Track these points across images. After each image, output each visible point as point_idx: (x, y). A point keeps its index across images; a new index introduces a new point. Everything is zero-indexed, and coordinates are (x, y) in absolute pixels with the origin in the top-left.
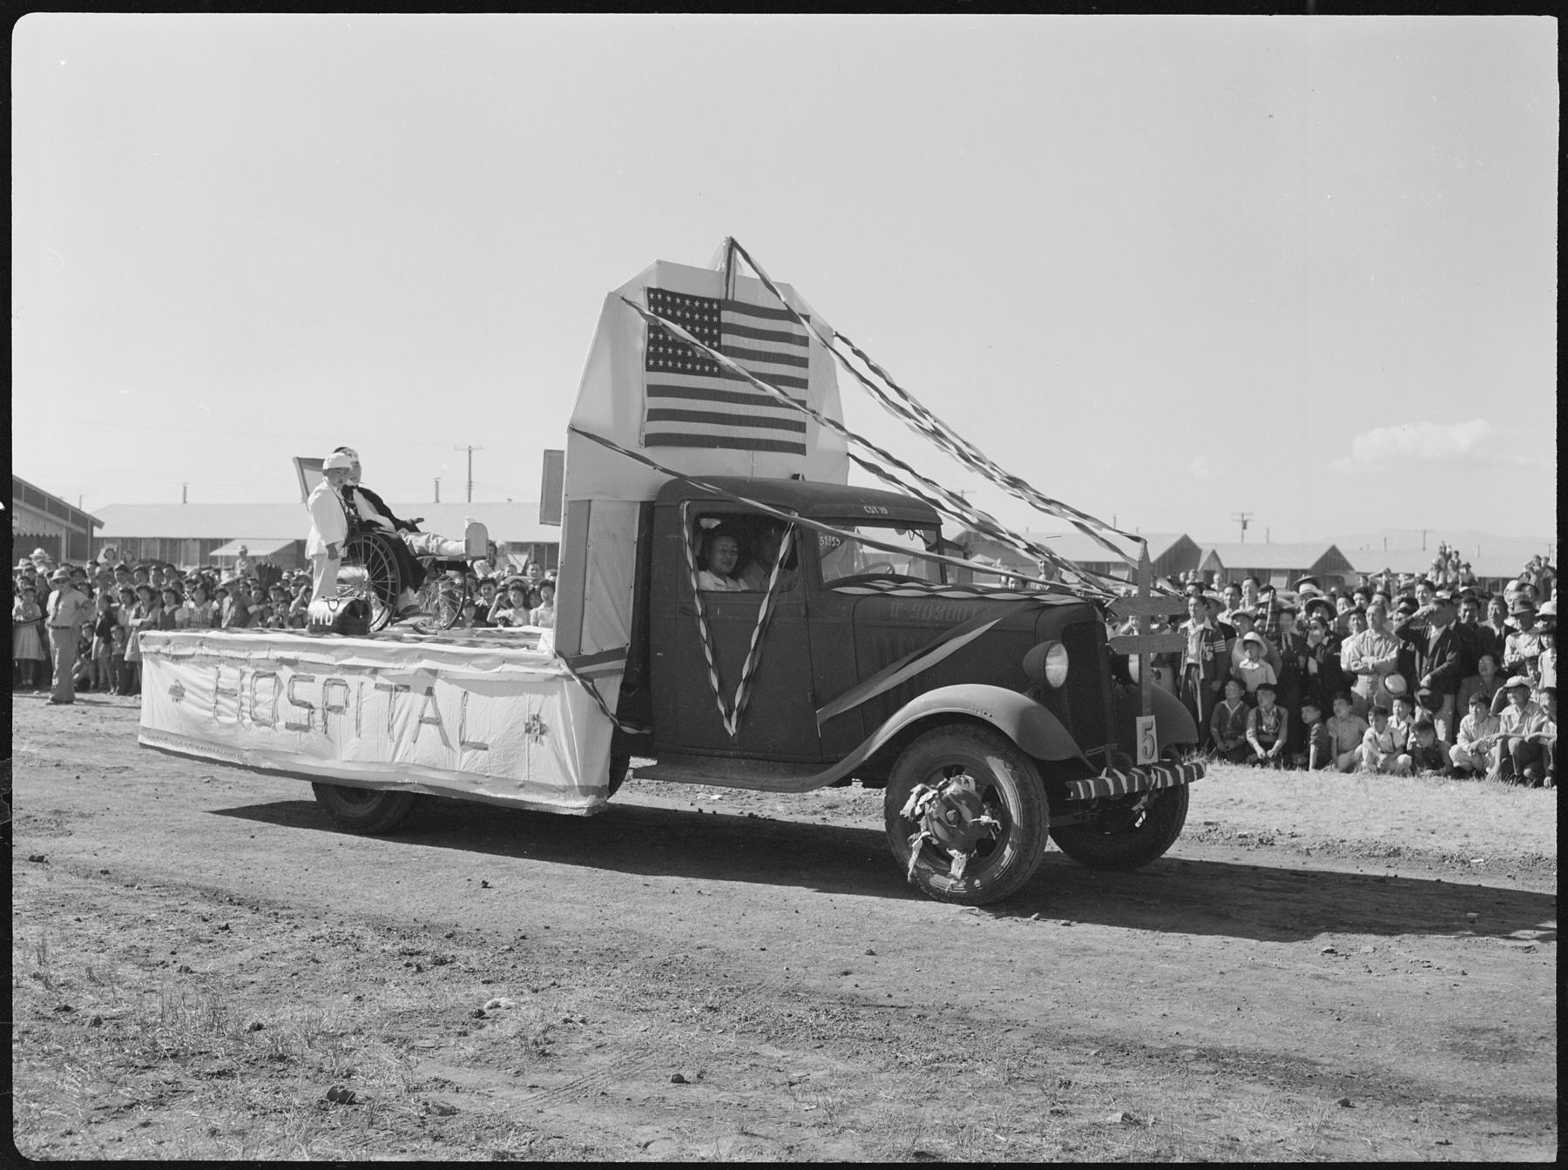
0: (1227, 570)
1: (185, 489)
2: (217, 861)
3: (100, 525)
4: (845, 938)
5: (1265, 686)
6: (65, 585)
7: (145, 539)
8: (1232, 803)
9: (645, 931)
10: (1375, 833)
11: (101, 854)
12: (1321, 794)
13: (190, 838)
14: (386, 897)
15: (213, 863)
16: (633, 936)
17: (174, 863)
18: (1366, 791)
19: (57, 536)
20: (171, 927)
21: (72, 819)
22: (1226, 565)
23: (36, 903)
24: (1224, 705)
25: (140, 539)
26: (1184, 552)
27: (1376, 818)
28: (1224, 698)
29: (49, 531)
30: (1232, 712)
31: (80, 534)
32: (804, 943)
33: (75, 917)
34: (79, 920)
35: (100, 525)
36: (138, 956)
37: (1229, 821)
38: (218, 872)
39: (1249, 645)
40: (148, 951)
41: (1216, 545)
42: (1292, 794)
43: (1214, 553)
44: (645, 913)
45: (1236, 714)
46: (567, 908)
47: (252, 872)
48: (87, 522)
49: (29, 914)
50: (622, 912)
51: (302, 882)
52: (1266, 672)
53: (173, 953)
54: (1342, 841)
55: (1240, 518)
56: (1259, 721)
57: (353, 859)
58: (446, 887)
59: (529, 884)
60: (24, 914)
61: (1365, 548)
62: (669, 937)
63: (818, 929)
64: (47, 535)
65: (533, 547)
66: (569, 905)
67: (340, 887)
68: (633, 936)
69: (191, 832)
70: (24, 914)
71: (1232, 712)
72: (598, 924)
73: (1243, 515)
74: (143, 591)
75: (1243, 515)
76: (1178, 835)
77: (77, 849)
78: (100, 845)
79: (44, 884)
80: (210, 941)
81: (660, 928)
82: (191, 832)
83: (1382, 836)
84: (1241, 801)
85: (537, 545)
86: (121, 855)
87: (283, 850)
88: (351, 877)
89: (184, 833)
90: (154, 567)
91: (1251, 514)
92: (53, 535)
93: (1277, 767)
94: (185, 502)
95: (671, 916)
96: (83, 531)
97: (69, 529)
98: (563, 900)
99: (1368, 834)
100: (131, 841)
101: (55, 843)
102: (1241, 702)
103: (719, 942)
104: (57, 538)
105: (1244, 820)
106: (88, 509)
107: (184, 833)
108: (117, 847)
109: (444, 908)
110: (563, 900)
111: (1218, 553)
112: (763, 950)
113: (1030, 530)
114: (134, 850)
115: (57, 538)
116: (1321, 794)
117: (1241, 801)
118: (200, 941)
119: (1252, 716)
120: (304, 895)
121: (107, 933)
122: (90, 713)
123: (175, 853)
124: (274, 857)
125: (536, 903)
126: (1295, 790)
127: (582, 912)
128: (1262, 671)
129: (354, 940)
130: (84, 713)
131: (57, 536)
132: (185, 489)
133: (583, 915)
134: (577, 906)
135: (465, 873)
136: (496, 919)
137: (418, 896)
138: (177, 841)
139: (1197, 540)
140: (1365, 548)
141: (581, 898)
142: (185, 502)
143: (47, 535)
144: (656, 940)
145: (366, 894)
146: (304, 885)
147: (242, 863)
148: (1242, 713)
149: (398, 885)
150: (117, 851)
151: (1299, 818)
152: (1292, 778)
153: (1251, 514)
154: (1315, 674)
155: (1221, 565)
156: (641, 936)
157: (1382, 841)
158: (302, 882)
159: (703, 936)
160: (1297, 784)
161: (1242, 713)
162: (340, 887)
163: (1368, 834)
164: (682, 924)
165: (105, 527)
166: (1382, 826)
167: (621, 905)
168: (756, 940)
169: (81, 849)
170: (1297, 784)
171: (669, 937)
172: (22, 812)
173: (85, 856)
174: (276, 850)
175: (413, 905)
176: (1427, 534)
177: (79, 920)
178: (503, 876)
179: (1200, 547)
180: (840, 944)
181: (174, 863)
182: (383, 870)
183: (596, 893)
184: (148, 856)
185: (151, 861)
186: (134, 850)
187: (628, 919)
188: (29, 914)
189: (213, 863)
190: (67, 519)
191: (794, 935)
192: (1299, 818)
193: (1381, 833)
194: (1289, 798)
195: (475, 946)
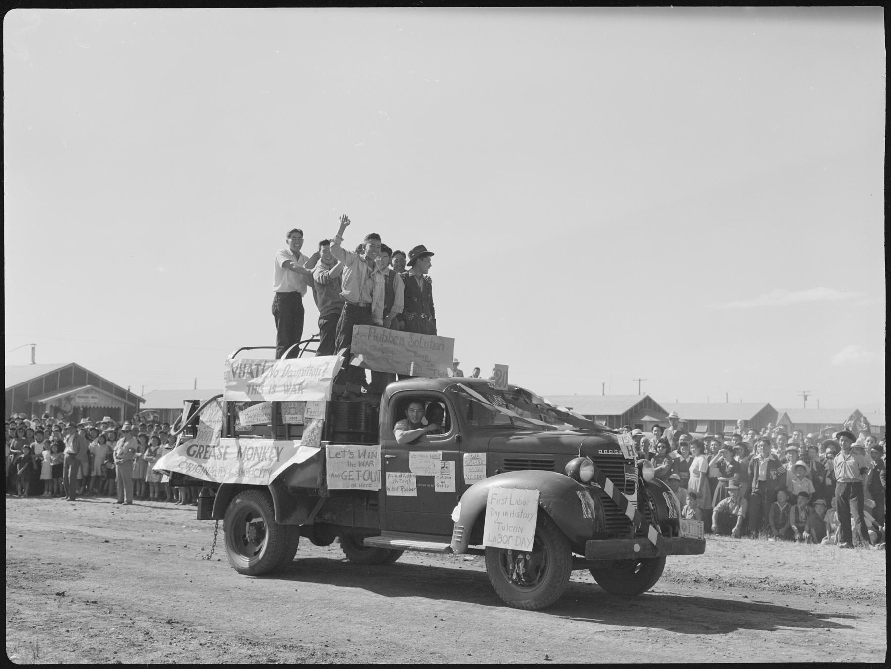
0: (794, 424)
1: (196, 381)
2: (161, 596)
3: (144, 401)
4: (521, 649)
5: (803, 494)
6: (128, 434)
7: (173, 409)
8: (779, 564)
9: (401, 642)
10: (863, 584)
11: (97, 591)
12: (834, 559)
13: (151, 582)
14: (253, 619)
15: (159, 597)
16: (393, 646)
17: (136, 597)
18: (861, 557)
19: (119, 408)
20: (121, 637)
21: (88, 570)
22: (793, 421)
23: (46, 621)
24: (777, 505)
25: (170, 410)
26: (767, 414)
27: (865, 574)
28: (776, 500)
29: (114, 405)
30: (781, 509)
31: (131, 406)
32: (495, 651)
33: (66, 629)
34: (68, 631)
35: (144, 401)
36: (94, 654)
37: (774, 576)
38: (160, 603)
39: (799, 468)
40: (101, 651)
41: (786, 409)
42: (816, 559)
43: (786, 414)
44: (404, 631)
45: (784, 509)
46: (358, 628)
47: (179, 603)
48: (136, 400)
49: (40, 627)
50: (390, 631)
51: (207, 609)
52: (809, 485)
53: (115, 653)
54: (842, 589)
55: (803, 394)
56: (797, 512)
57: (240, 596)
58: (289, 614)
59: (339, 613)
60: (37, 627)
61: (877, 411)
62: (414, 646)
63: (506, 642)
64: (114, 407)
65: (608, 417)
66: (360, 626)
67: (228, 613)
68: (393, 646)
69: (152, 578)
70: (37, 627)
71: (781, 509)
72: (374, 638)
73: (804, 392)
74: (142, 438)
75: (804, 392)
76: (660, 575)
77: (84, 588)
78: (98, 586)
79: (55, 610)
80: (140, 645)
81: (411, 640)
82: (152, 578)
83: (867, 586)
84: (784, 563)
85: (711, 421)
86: (108, 592)
87: (201, 590)
88: (235, 607)
89: (146, 579)
90: (156, 424)
91: (809, 392)
92: (117, 407)
93: (808, 542)
94: (195, 389)
95: (419, 633)
96: (133, 405)
97: (125, 403)
98: (358, 623)
99: (859, 584)
100: (116, 584)
101: (73, 584)
102: (787, 503)
103: (444, 650)
104: (119, 409)
105: (783, 575)
106: (136, 391)
107: (146, 579)
108: (107, 587)
109: (285, 627)
110: (358, 623)
111: (788, 414)
112: (470, 655)
113: (743, 401)
114: (116, 589)
115: (119, 409)
116: (834, 559)
117: (784, 563)
118: (134, 645)
119: (793, 509)
120: (206, 618)
121: (82, 639)
122: (121, 508)
123: (139, 591)
124: (194, 594)
125: (341, 624)
126: (818, 556)
127: (366, 630)
128: (806, 484)
129: (225, 646)
130: (118, 508)
131: (119, 408)
132: (196, 381)
133: (367, 632)
134: (364, 627)
135: (303, 606)
136: (314, 634)
137: (272, 619)
138: (142, 584)
139: (775, 406)
140: (877, 411)
141: (368, 621)
142: (195, 389)
143: (114, 407)
144: (406, 648)
145: (242, 618)
146: (207, 612)
147: (175, 598)
148: (787, 509)
149: (262, 613)
150: (106, 589)
151: (817, 574)
152: (817, 549)
153: (809, 392)
154: (829, 486)
155: (790, 422)
156: (397, 645)
157: (867, 589)
158: (207, 609)
159: (435, 646)
160: (819, 553)
161: (787, 509)
162: (228, 613)
163: (859, 584)
164: (424, 639)
165: (146, 403)
166: (868, 579)
167: (391, 626)
168: (467, 649)
169: (86, 588)
170: (819, 553)
171: (414, 646)
172: (60, 566)
173: (87, 593)
174: (197, 590)
175: (267, 625)
176: (144, 388)
177: (68, 631)
178: (325, 607)
179: (778, 410)
180: (517, 652)
181: (136, 597)
182: (256, 603)
183: (378, 619)
184: (123, 593)
185: (123, 596)
186: (116, 589)
187: (393, 634)
188: (40, 627)
189: (159, 597)
190: (125, 398)
191: (491, 646)
192: (817, 574)
193: (866, 584)
194: (814, 561)
195: (296, 651)
